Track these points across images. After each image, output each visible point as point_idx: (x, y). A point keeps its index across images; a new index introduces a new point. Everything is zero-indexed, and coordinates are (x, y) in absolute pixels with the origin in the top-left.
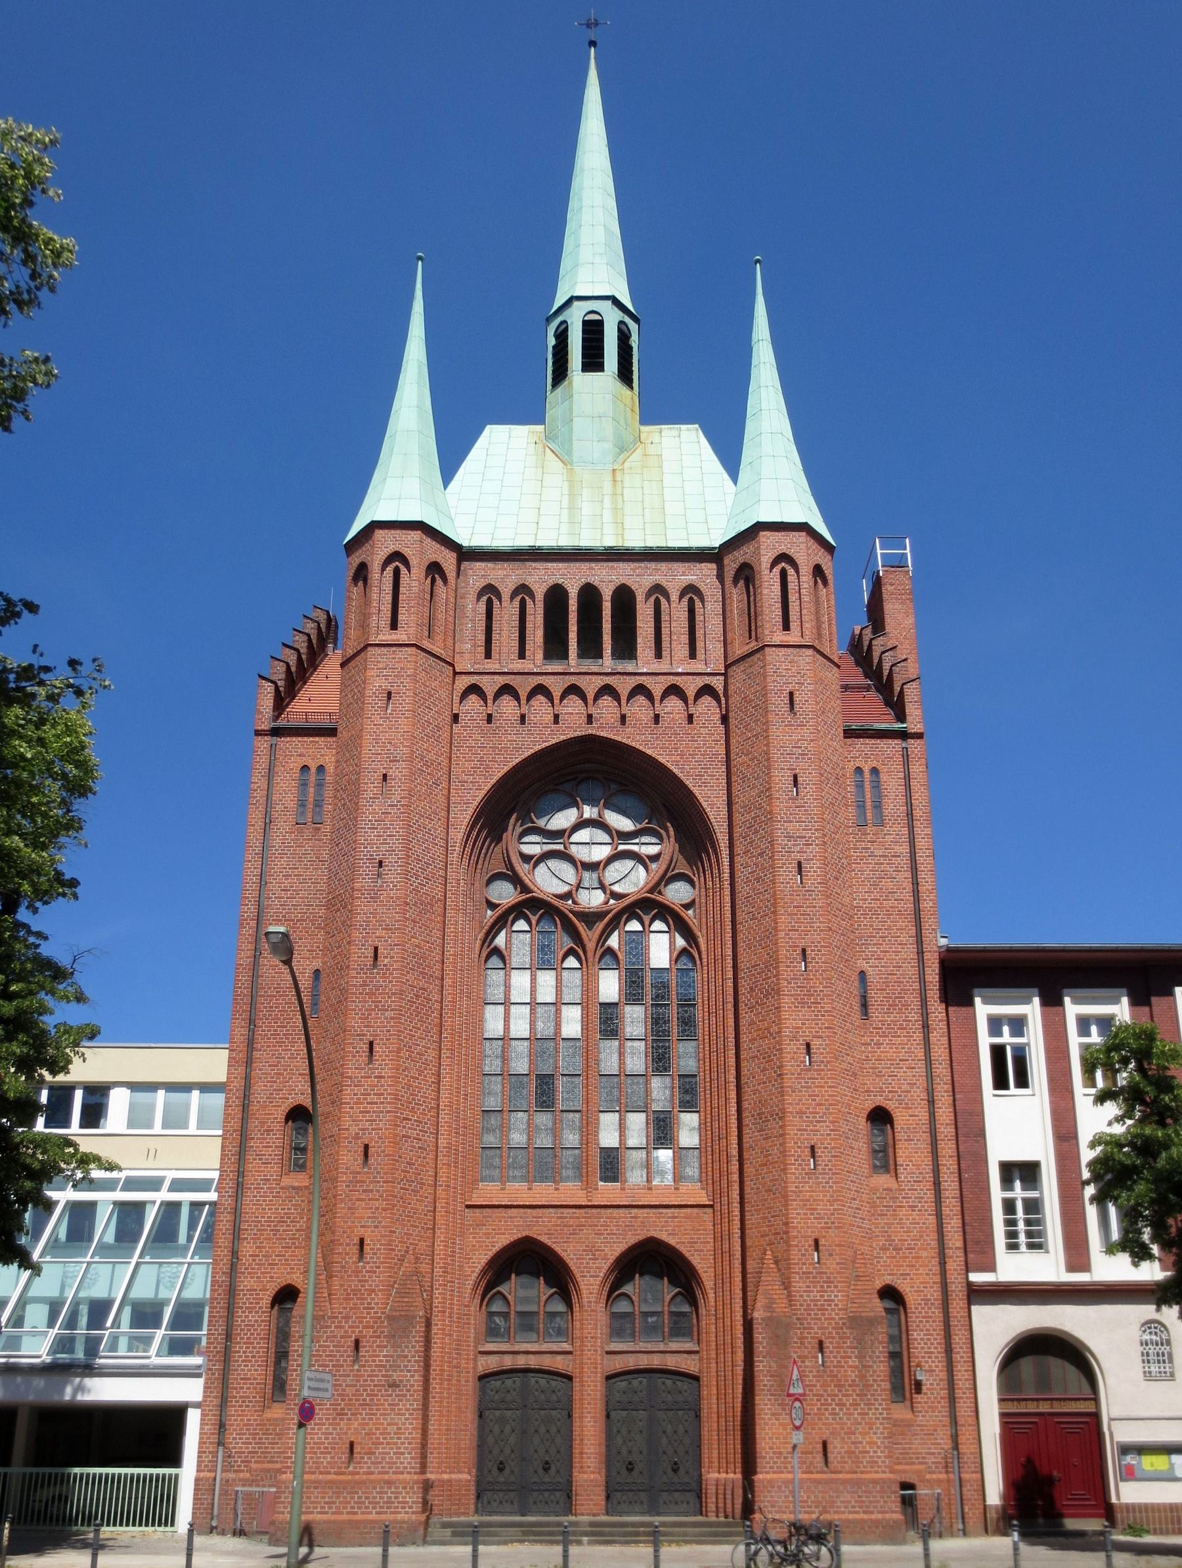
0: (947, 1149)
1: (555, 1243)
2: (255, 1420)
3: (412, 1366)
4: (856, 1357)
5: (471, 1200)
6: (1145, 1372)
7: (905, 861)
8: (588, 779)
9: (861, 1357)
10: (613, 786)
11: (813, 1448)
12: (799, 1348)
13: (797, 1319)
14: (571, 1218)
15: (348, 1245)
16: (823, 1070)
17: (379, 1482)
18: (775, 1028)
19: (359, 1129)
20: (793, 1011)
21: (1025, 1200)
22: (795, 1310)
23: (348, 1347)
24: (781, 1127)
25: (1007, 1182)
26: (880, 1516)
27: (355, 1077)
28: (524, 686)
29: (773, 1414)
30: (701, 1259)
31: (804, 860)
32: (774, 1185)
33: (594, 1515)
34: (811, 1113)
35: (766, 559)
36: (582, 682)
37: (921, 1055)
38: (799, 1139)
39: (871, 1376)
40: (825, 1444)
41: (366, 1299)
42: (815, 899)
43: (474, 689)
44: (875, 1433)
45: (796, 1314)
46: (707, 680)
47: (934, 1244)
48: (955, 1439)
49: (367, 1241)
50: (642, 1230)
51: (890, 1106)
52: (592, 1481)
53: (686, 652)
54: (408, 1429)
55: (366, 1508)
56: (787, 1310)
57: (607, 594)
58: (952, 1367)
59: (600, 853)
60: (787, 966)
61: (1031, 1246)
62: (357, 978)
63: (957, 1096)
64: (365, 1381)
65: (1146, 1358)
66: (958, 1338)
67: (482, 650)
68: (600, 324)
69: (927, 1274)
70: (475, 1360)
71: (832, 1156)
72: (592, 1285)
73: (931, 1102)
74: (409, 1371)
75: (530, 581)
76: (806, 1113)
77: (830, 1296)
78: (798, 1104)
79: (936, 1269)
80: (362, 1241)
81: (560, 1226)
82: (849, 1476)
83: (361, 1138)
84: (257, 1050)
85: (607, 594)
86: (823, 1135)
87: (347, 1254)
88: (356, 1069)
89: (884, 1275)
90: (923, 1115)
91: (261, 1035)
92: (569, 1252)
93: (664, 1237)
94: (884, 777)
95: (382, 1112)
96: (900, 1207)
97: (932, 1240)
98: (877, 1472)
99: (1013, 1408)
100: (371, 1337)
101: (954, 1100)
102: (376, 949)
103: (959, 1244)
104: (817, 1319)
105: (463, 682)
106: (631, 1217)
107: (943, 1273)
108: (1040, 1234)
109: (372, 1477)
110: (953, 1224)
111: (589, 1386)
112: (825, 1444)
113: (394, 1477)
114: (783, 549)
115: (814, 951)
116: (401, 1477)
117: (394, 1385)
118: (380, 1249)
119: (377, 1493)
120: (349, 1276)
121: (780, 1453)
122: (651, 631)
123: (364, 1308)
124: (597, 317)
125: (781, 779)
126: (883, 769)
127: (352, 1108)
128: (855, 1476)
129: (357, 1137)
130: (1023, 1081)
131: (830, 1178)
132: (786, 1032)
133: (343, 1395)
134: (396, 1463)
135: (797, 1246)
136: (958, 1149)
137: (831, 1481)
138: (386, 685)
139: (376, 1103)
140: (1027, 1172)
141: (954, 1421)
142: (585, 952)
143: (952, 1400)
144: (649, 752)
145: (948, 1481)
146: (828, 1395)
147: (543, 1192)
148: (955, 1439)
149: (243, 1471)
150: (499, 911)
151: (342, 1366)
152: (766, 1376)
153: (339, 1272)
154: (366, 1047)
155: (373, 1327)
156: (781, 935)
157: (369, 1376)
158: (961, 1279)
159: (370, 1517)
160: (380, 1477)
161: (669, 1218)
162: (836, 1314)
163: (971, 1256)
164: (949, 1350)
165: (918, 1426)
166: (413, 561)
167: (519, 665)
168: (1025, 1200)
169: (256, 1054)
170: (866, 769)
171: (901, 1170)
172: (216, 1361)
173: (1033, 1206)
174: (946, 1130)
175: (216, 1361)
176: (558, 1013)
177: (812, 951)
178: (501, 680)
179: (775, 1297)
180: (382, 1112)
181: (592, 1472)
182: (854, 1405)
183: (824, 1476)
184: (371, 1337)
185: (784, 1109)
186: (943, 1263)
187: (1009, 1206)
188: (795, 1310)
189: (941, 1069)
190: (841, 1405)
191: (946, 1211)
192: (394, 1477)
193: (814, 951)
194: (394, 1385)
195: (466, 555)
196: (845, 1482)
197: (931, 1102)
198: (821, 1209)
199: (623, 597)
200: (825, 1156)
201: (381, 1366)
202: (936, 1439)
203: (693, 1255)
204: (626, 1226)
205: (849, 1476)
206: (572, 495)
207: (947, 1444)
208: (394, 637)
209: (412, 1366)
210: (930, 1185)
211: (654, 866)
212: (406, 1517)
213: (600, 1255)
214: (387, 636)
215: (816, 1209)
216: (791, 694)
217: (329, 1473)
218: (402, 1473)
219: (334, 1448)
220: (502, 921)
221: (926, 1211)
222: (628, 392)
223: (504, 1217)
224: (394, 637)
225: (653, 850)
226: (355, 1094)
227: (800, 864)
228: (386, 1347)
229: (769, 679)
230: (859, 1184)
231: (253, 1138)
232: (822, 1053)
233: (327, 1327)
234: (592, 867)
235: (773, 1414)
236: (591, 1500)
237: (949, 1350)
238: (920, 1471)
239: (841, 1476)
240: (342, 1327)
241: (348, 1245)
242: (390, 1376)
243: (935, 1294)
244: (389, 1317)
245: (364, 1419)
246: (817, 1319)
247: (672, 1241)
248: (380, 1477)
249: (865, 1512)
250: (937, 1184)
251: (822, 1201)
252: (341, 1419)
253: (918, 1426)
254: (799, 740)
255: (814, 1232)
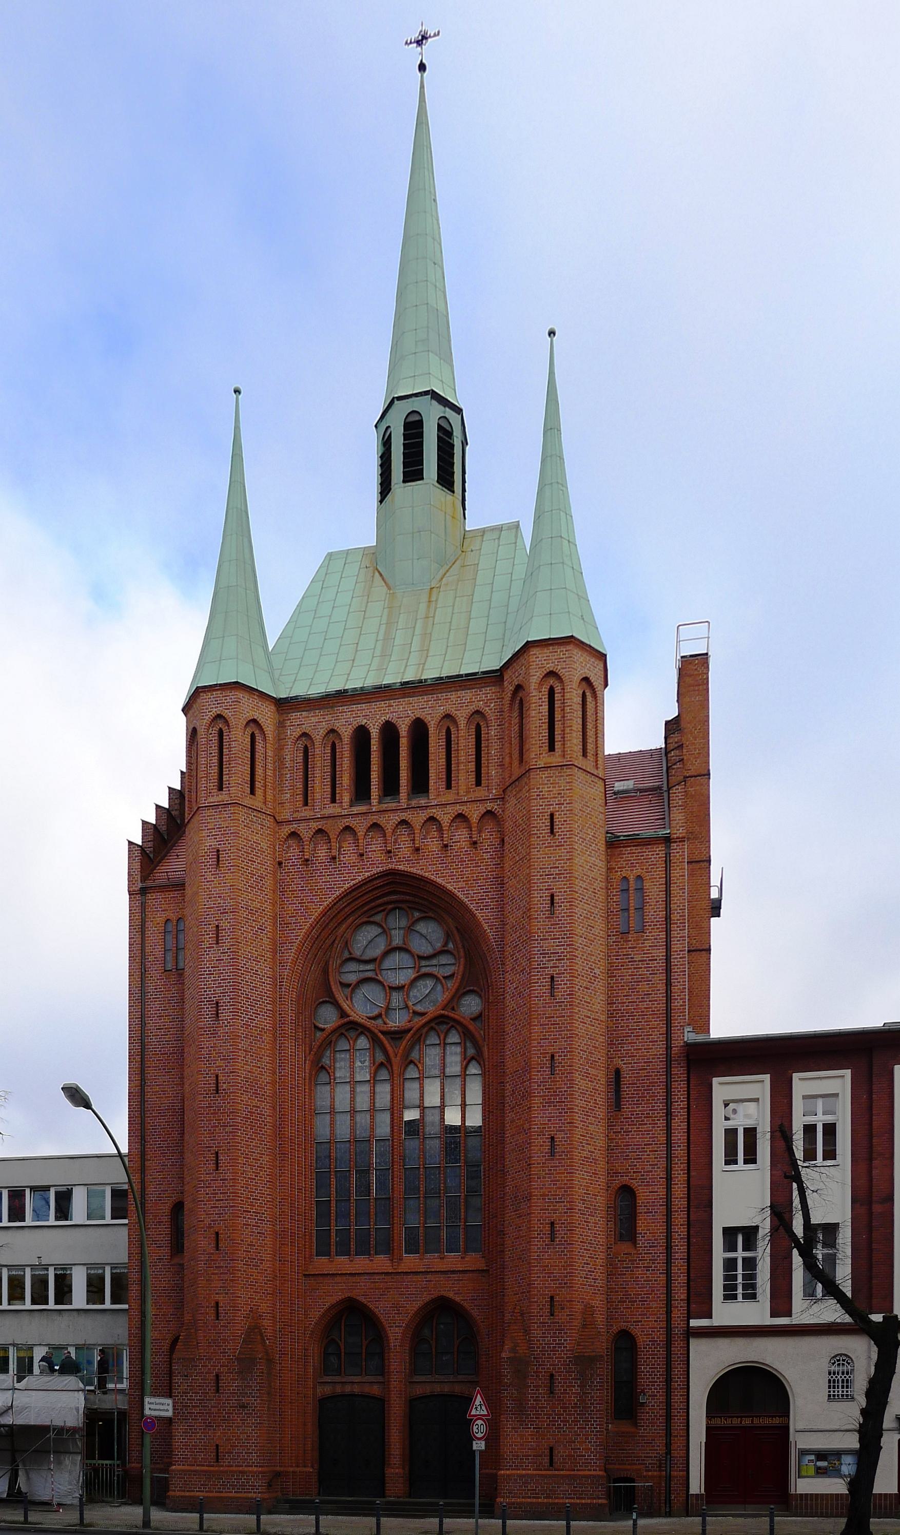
0: (680, 1219)
1: (369, 1302)
2: (164, 1430)
3: (255, 1393)
4: (578, 1386)
5: (307, 1271)
6: (829, 1396)
7: (660, 964)
8: (394, 909)
9: (582, 1386)
10: (417, 914)
11: (542, 1452)
12: (535, 1379)
13: (534, 1358)
14: (381, 1282)
15: (208, 1307)
16: (564, 1159)
17: (236, 1472)
18: (526, 1126)
19: (211, 1221)
20: (541, 1110)
21: (744, 1259)
22: (533, 1351)
23: (211, 1380)
24: (529, 1207)
25: (730, 1246)
26: (589, 1501)
27: (207, 1181)
28: (335, 829)
29: (513, 1428)
30: (480, 1312)
31: (557, 974)
32: (523, 1254)
33: (399, 1497)
34: (551, 1195)
35: (535, 676)
36: (382, 820)
37: (663, 1139)
38: (541, 1217)
39: (589, 1400)
40: (551, 1449)
41: (222, 1346)
42: (564, 1009)
43: (294, 835)
44: (590, 1442)
45: (534, 1354)
46: (489, 806)
47: (663, 1297)
48: (668, 1445)
49: (221, 1304)
50: (435, 1291)
51: (634, 1184)
52: (397, 1474)
53: (472, 779)
54: (254, 1436)
55: (228, 1489)
56: (527, 1351)
57: (404, 730)
58: (667, 1392)
59: (403, 978)
60: (538, 1072)
61: (745, 1297)
62: (204, 1101)
63: (692, 1174)
64: (223, 1403)
65: (832, 1384)
66: (677, 1371)
67: (300, 798)
68: (420, 424)
69: (655, 1321)
70: (314, 1388)
71: (567, 1230)
72: (397, 1333)
73: (669, 1179)
74: (253, 1397)
75: (337, 725)
76: (548, 1195)
77: (561, 1340)
78: (542, 1188)
79: (663, 1317)
80: (217, 1303)
81: (372, 1289)
82: (568, 1473)
83: (213, 1227)
84: (148, 1160)
85: (404, 730)
86: (561, 1213)
87: (208, 1314)
88: (207, 1174)
89: (620, 1322)
90: (662, 1192)
91: (149, 1148)
92: (380, 1308)
93: (451, 1295)
94: (647, 885)
95: (227, 1207)
96: (637, 1267)
97: (661, 1292)
98: (590, 1470)
99: (717, 1422)
100: (226, 1373)
101: (689, 1178)
102: (217, 1076)
103: (684, 1296)
104: (550, 1358)
105: (286, 830)
106: (426, 1281)
107: (669, 1320)
108: (753, 1286)
109: (231, 1469)
110: (680, 1279)
111: (395, 1407)
112: (551, 1449)
113: (246, 1469)
114: (550, 667)
115: (561, 1056)
116: (250, 1469)
117: (243, 1407)
118: (230, 1310)
119: (235, 1479)
120: (209, 1330)
121: (517, 1456)
122: (443, 761)
123: (221, 1353)
124: (417, 418)
125: (540, 899)
126: (647, 876)
127: (206, 1204)
128: (572, 1473)
129: (210, 1227)
130: (750, 1158)
131: (564, 1248)
132: (535, 1128)
133: (210, 1413)
134: (247, 1459)
135: (536, 1302)
136: (688, 1217)
137: (554, 1476)
138: (214, 843)
139: (222, 1200)
140: (750, 1234)
141: (668, 1434)
142: (391, 1066)
143: (669, 1417)
144: (439, 880)
145: (660, 1477)
146: (555, 1415)
147: (361, 1263)
148: (668, 1445)
149: (158, 1463)
150: (324, 1034)
151: (208, 1393)
152: (509, 1400)
153: (202, 1326)
154: (213, 1157)
155: (227, 1366)
156: (535, 1043)
157: (226, 1400)
158: (683, 1324)
159: (230, 1495)
160: (237, 1469)
161: (455, 1280)
162: (564, 1354)
163: (693, 1306)
164: (669, 1380)
165: (639, 1436)
166: (232, 721)
167: (332, 810)
168: (744, 1259)
169: (148, 1163)
170: (632, 878)
171: (639, 1237)
172: (137, 1389)
173: (750, 1264)
174: (679, 1203)
175: (137, 1389)
176: (372, 1118)
177: (559, 1056)
178: (315, 825)
179: (519, 1341)
180: (227, 1207)
181: (397, 1468)
182: (576, 1421)
183: (550, 1472)
184: (226, 1373)
185: (531, 1193)
186: (669, 1313)
187: (730, 1264)
188: (533, 1351)
189: (680, 1151)
190: (565, 1421)
191: (675, 1270)
192: (246, 1469)
193: (561, 1056)
194: (243, 1407)
195: (285, 705)
196: (563, 1476)
197: (669, 1179)
198: (556, 1273)
199: (419, 729)
200: (562, 1230)
201: (235, 1393)
202: (654, 1446)
203: (473, 1309)
204: (422, 1288)
205: (568, 1473)
206: (390, 624)
207: (662, 1450)
208: (220, 798)
209: (255, 1393)
210: (662, 1249)
211: (450, 984)
212: (254, 1495)
213: (402, 1310)
214: (215, 799)
215: (553, 1273)
216: (552, 816)
217: (203, 1465)
218: (252, 1466)
219: (206, 1449)
220: (329, 1043)
221: (657, 1270)
222: (449, 497)
223: (332, 1283)
224: (220, 798)
225: (448, 971)
226: (207, 1194)
227: (552, 978)
228: (237, 1380)
229: (533, 803)
230: (594, 1251)
231: (150, 1228)
232: (564, 1145)
233: (196, 1366)
234: (400, 988)
235: (513, 1428)
236: (396, 1487)
237: (669, 1380)
238: (640, 1470)
239: (562, 1472)
240: (207, 1366)
241: (208, 1307)
242: (240, 1400)
243: (661, 1336)
244: (237, 1359)
245: (225, 1429)
246: (550, 1358)
247: (457, 1299)
248: (237, 1469)
249: (578, 1498)
250: (669, 1248)
251: (559, 1266)
252: (209, 1430)
253: (639, 1436)
254: (557, 860)
255: (551, 1291)
